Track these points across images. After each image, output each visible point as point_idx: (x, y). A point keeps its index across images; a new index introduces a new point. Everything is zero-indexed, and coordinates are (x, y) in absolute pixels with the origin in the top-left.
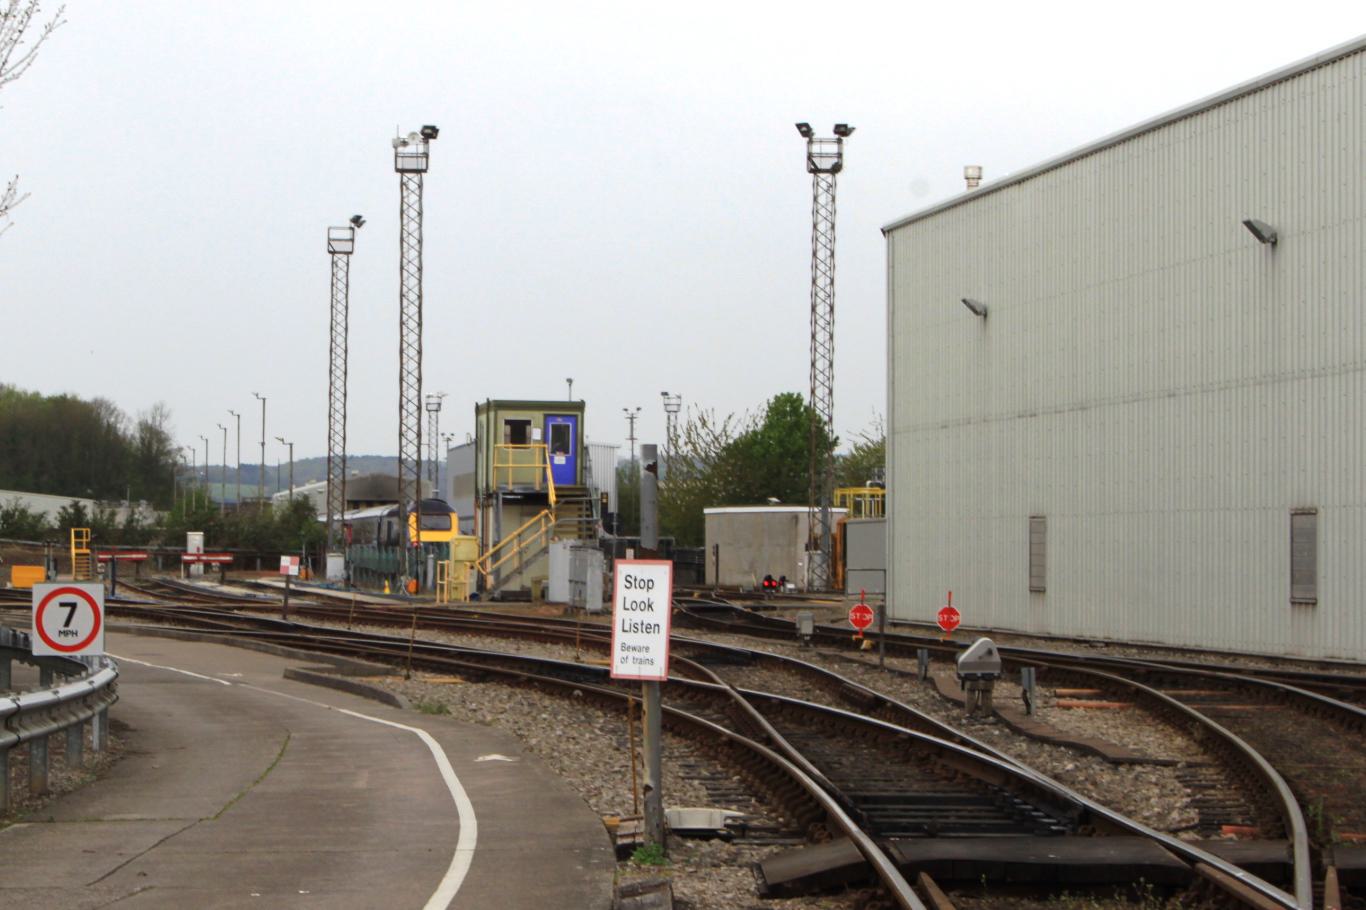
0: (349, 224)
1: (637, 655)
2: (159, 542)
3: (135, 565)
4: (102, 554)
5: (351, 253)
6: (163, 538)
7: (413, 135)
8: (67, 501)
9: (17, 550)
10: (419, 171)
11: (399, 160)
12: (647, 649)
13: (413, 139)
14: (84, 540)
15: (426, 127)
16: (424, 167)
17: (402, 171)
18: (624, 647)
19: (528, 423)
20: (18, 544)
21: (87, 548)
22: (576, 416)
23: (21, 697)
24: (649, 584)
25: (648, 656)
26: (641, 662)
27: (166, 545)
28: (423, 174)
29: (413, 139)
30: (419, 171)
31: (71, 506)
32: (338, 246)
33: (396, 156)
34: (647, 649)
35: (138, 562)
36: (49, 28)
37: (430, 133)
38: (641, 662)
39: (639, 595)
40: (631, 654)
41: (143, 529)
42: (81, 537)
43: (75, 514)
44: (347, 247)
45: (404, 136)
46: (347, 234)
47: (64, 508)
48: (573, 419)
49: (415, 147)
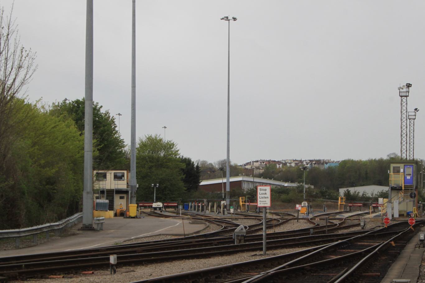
0: (414, 111)
1: (263, 202)
2: (372, 201)
3: (359, 207)
4: (350, 204)
5: (415, 119)
6: (373, 200)
7: (404, 86)
8: (345, 189)
9: (329, 203)
10: (406, 96)
11: (400, 93)
12: (266, 201)
13: (404, 87)
14: (344, 200)
15: (407, 84)
16: (407, 95)
17: (401, 96)
18: (260, 201)
19: (399, 167)
20: (330, 201)
21: (344, 202)
22: (413, 165)
23: (150, 211)
24: (265, 190)
25: (266, 203)
26: (264, 204)
27: (373, 202)
28: (408, 97)
29: (404, 87)
30: (406, 96)
31: (347, 191)
32: (410, 117)
33: (400, 92)
34: (266, 201)
35: (360, 206)
36: (35, 70)
37: (409, 86)
38: (264, 204)
39: (264, 192)
40: (262, 203)
41: (367, 197)
42: (343, 199)
43: (348, 193)
44: (414, 117)
45: (402, 86)
46: (413, 114)
47: (345, 191)
48: (412, 166)
49: (405, 90)
